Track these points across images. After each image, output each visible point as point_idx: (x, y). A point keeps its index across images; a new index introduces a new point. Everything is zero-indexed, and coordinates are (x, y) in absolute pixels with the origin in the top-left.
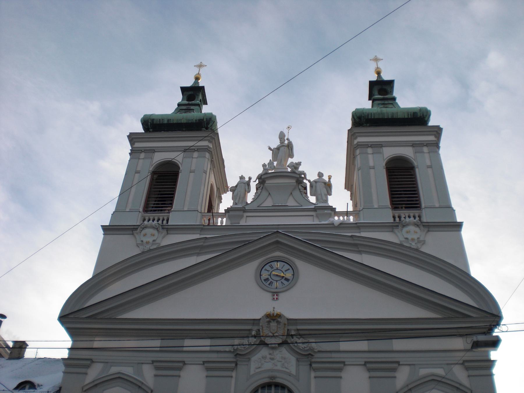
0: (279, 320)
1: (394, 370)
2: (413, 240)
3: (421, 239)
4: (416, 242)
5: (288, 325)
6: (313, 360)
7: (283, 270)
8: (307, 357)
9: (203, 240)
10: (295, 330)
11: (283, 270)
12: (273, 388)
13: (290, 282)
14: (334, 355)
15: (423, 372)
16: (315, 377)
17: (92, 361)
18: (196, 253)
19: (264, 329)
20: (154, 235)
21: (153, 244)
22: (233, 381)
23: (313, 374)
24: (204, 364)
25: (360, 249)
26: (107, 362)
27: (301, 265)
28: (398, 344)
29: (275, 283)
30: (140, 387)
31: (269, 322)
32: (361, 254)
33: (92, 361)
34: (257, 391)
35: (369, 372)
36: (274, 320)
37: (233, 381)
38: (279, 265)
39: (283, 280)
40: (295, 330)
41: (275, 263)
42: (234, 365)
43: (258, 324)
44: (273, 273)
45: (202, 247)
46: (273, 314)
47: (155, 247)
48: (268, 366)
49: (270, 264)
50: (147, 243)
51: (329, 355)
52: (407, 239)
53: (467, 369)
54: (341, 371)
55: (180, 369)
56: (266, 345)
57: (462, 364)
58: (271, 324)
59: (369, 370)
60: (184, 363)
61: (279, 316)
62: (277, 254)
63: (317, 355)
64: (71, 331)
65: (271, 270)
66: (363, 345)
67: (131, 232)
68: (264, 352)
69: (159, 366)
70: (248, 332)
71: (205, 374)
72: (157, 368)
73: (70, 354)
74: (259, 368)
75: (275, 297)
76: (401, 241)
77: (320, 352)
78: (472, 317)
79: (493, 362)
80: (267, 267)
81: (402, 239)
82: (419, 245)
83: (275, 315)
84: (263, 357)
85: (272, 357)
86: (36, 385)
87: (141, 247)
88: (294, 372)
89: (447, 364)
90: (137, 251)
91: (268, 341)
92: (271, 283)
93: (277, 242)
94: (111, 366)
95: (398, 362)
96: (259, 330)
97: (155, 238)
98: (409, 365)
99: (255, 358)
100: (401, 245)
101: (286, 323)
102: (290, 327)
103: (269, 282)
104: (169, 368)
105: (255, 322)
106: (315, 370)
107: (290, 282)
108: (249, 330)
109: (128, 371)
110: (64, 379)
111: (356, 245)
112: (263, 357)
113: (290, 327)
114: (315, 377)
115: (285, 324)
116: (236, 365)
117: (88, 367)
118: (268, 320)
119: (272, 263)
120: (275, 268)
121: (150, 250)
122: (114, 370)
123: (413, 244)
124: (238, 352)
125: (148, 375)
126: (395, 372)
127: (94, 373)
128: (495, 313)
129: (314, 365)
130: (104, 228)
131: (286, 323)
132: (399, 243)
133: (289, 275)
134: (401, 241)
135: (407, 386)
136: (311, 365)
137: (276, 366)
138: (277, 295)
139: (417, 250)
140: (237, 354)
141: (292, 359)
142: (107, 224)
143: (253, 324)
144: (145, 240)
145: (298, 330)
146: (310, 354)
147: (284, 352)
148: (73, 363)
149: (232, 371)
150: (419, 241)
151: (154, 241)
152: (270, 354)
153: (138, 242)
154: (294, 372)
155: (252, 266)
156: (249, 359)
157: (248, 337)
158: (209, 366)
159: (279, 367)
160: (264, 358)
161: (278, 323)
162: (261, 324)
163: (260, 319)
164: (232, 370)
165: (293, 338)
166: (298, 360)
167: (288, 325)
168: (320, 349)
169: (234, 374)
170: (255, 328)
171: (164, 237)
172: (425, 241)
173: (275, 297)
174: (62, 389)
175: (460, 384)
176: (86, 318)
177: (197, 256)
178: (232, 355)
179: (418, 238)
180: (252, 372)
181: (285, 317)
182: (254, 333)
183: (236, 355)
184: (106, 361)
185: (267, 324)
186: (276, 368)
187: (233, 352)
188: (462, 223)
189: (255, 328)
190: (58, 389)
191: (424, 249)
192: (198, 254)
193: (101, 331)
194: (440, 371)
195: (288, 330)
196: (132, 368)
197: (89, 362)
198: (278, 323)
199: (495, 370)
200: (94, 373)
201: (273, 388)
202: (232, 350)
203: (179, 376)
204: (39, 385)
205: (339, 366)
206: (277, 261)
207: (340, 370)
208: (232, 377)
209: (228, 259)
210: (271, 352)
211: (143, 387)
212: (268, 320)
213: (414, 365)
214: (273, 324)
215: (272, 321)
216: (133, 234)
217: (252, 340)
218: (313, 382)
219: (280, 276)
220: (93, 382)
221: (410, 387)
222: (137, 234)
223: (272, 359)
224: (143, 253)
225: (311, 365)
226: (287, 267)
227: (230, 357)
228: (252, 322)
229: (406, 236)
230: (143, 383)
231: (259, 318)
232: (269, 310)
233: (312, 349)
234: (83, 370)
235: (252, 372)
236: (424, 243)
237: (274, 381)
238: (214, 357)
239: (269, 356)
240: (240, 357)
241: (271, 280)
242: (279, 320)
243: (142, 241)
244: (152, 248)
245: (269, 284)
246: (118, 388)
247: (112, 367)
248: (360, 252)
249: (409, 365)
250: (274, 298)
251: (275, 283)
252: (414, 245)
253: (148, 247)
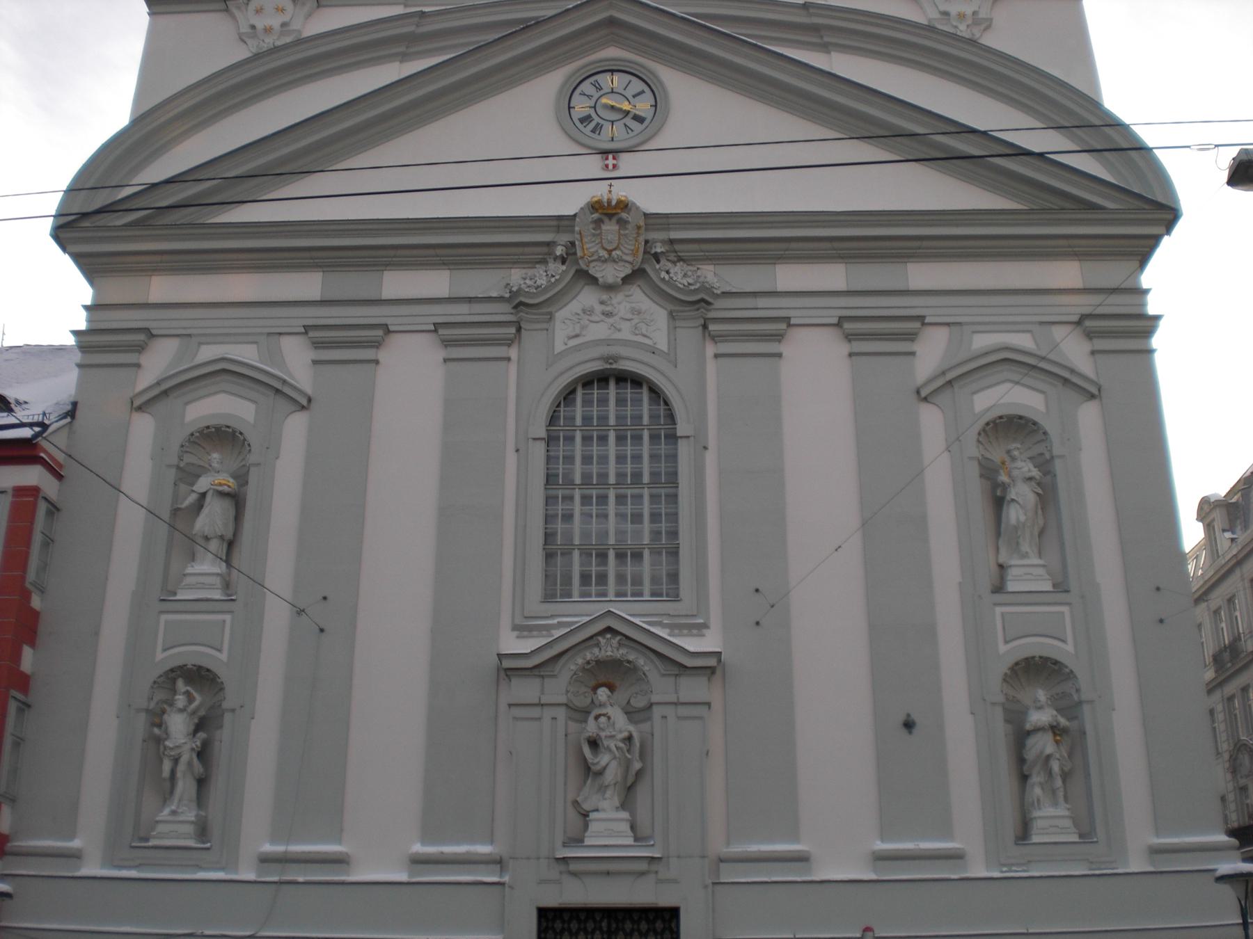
0: (624, 215)
1: (911, 337)
2: (962, 16)
3: (982, 15)
4: (970, 22)
5: (646, 230)
6: (711, 315)
7: (629, 93)
8: (695, 307)
9: (416, 19)
10: (663, 242)
11: (629, 93)
12: (612, 384)
13: (646, 125)
14: (762, 302)
15: (982, 341)
16: (716, 356)
17: (150, 334)
18: (396, 55)
19: (585, 240)
20: (283, 10)
21: (282, 34)
22: (513, 368)
23: (710, 349)
24: (436, 331)
25: (826, 39)
26: (190, 335)
27: (675, 82)
28: (921, 275)
29: (607, 126)
30: (278, 391)
31: (598, 223)
32: (828, 52)
33: (150, 334)
34: (573, 391)
35: (850, 341)
36: (610, 216)
37: (513, 368)
38: (617, 81)
39: (628, 121)
40: (663, 242)
41: (608, 76)
42: (513, 330)
43: (571, 229)
44: (604, 100)
45: (412, 39)
46: (609, 201)
47: (288, 40)
48: (598, 331)
49: (592, 80)
50: (268, 30)
51: (749, 302)
52: (946, 14)
53: (1090, 335)
54: (780, 341)
55: (376, 344)
56: (593, 280)
57: (838, 325)
58: (604, 227)
59: (850, 337)
60: (387, 331)
61: (624, 205)
62: (612, 52)
63: (719, 303)
64: (90, 266)
65: (596, 95)
66: (832, 276)
67: (222, 6)
68: (587, 297)
69: (324, 339)
70: (545, 249)
71: (441, 354)
72: (318, 345)
73: (89, 321)
74: (577, 336)
75: (611, 162)
76: (930, 20)
77: (726, 294)
78: (1102, 208)
79: (1146, 292)
80: (586, 87)
81: (933, 14)
82: (976, 32)
83: (614, 203)
84: (584, 311)
85: (608, 309)
86: (12, 401)
87: (249, 41)
88: (663, 345)
89: (1041, 323)
90: (242, 53)
91: (596, 270)
92: (597, 129)
93: (611, 22)
94: (200, 344)
95: (921, 319)
96: (573, 244)
97: (286, 18)
98: (948, 324)
99: (566, 314)
100: (930, 28)
101: (642, 223)
102: (652, 235)
103: (592, 125)
104: (350, 341)
105: (562, 223)
106: (715, 338)
107: (646, 123)
108: (548, 244)
109: (247, 354)
110: (81, 384)
111: (815, 29)
112: (584, 311)
113: (652, 235)
114: (716, 356)
115: (639, 228)
116: (519, 329)
117: (140, 348)
118: (596, 216)
119: (599, 77)
120: (606, 90)
121: (275, 50)
122: (207, 353)
123: (962, 27)
124: (523, 299)
125: (297, 362)
126: (913, 340)
127: (158, 362)
128: (1160, 199)
129: (712, 327)
130: (86, 308)
131: (642, 223)
132: (926, 23)
133: (643, 106)
134: (930, 20)
135: (944, 373)
136: (705, 327)
137: (619, 330)
138: (614, 158)
139: (973, 42)
140: (521, 304)
141: (659, 315)
142: (89, 303)
143: (558, 229)
144: (260, 23)
145: (672, 242)
146: (703, 300)
147: (637, 296)
148: (102, 342)
149: (509, 345)
150: (976, 20)
151: (284, 25)
152: (602, 303)
153: (243, 30)
154: (663, 345)
155: (551, 82)
156: (551, 317)
157: (544, 262)
158: (451, 336)
159: (626, 334)
160: (588, 311)
161: (622, 223)
162: (577, 229)
163: (575, 215)
164: (509, 342)
165: (658, 262)
166: (671, 314)
167: (646, 230)
168: (728, 289)
169: (513, 353)
170: (564, 238)
171: (309, 15)
172: (991, 20)
173: (611, 162)
174: (79, 406)
175: (1072, 371)
176: (125, 225)
177: (401, 62)
178: (506, 308)
179: (974, 13)
180: (559, 347)
181: (638, 208)
182: (559, 251)
183: (515, 307)
184: (188, 332)
185: (592, 226)
186: (617, 336)
187: (508, 300)
188: (1157, 318)
189: (564, 238)
190: (69, 407)
191: (988, 40)
192: (404, 57)
193: (166, 258)
194: (1023, 341)
195: (647, 242)
196: (255, 346)
197: (142, 337)
198: (622, 223)
199: (1156, 341)
200: (158, 362)
201: (612, 384)
202: (507, 295)
203: (377, 362)
204: (18, 403)
205: (774, 330)
206: (612, 71)
207: (778, 337)
208: (509, 359)
209: (485, 65)
210: (605, 297)
211: (286, 390)
212: (596, 216)
213: (960, 324)
214: (610, 227)
215: (606, 219)
216: (227, 10)
217: (556, 268)
218: (711, 366)
219: (620, 110)
220: (158, 383)
221: (949, 376)
222: (239, 8)
223: (608, 314)
224: (257, 57)
225: (705, 327)
226: (637, 85)
227: (502, 312)
228: (554, 223)
229: (942, 8)
230: (284, 382)
231: (572, 213)
232: (598, 191)
233: (708, 289)
234: (367, 354)
235: (559, 347)
236: (988, 25)
237: (614, 366)
238: (460, 312)
239: (599, 308)
240: (525, 310)
241: (597, 120)
242: (624, 215)
243: (253, 27)
244: (278, 43)
245: (593, 131)
246: (222, 396)
247: (204, 348)
248: (825, 48)
249: (948, 324)
250: (607, 166)
251: (607, 126)
252: (963, 30)
253: (269, 42)
